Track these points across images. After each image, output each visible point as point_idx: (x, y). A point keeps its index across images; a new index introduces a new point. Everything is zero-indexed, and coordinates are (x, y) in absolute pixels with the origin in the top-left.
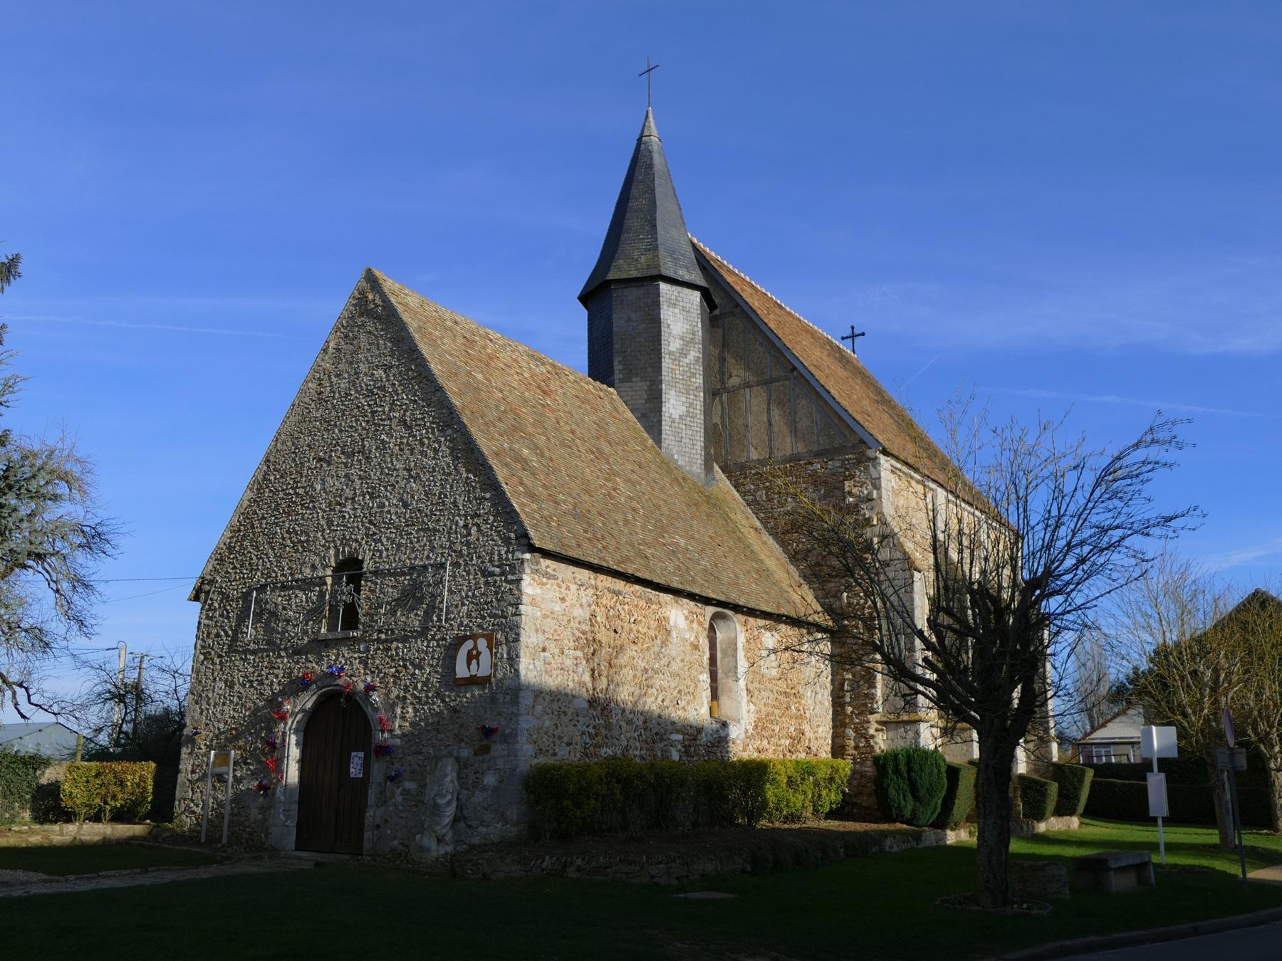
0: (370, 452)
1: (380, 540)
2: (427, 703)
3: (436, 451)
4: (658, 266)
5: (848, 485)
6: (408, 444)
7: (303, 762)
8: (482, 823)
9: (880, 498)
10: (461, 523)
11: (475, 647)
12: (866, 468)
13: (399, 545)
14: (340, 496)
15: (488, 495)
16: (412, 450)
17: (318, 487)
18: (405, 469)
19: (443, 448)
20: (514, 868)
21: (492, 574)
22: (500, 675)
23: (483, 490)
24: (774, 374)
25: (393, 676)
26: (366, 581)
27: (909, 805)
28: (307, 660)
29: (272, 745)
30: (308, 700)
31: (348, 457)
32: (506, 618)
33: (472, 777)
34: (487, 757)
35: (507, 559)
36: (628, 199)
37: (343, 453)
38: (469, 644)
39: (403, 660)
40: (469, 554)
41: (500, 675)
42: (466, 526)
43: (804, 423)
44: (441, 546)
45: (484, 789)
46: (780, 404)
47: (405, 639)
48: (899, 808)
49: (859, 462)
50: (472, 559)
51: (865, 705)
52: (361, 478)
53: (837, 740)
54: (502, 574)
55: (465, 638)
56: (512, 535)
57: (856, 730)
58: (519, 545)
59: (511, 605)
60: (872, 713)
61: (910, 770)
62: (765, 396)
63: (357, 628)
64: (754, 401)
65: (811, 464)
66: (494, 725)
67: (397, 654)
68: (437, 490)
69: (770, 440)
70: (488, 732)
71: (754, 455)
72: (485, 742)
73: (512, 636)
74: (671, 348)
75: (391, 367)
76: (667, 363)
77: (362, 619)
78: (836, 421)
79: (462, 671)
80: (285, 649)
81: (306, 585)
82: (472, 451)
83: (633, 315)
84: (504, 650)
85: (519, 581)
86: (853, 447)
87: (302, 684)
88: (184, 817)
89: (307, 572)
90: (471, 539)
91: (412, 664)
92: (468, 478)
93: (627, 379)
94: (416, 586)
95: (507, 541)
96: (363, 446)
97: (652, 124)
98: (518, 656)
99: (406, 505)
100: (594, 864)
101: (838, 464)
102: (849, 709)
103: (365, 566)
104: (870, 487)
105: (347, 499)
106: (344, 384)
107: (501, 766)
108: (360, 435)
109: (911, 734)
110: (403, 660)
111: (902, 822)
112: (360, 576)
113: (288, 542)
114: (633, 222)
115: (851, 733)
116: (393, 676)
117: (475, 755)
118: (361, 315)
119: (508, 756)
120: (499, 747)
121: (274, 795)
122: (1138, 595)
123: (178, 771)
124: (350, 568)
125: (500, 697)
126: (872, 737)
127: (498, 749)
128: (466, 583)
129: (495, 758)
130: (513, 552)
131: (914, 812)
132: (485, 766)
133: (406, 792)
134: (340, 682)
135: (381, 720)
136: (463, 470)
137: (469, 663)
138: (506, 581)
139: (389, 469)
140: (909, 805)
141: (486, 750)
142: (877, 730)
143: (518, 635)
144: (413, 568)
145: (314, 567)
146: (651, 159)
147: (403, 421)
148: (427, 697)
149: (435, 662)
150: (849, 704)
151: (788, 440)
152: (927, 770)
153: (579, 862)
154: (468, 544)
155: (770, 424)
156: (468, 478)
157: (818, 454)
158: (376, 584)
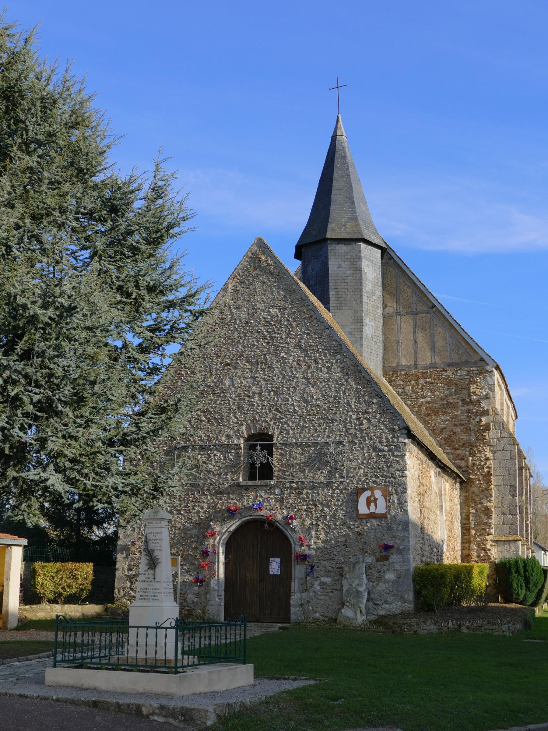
0: (272, 363)
1: (286, 423)
2: (334, 529)
3: (329, 369)
4: (360, 232)
5: (473, 387)
6: (304, 361)
7: (226, 564)
8: (386, 602)
9: (494, 397)
10: (354, 417)
11: (373, 495)
12: (485, 377)
13: (303, 427)
14: (248, 391)
15: (375, 401)
16: (309, 367)
17: (228, 383)
18: (304, 378)
19: (335, 367)
20: (432, 628)
21: (382, 451)
22: (393, 513)
23: (370, 397)
24: (419, 309)
25: (305, 511)
26: (277, 449)
27: (523, 593)
28: (229, 498)
29: (205, 553)
30: (233, 525)
31: (252, 365)
32: (395, 478)
33: (376, 575)
34: (386, 563)
35: (393, 442)
36: (331, 180)
37: (247, 362)
38: (368, 493)
39: (313, 500)
40: (362, 437)
41: (393, 513)
42: (358, 419)
43: (440, 344)
44: (339, 430)
45: (386, 582)
46: (423, 329)
47: (313, 488)
48: (518, 594)
49: (480, 373)
50: (365, 440)
51: (485, 529)
52: (265, 380)
53: (464, 551)
54: (389, 451)
55: (364, 490)
56: (396, 427)
57: (478, 545)
58: (401, 433)
59: (399, 470)
60: (489, 534)
61: (526, 571)
62: (411, 323)
63: (272, 479)
64: (403, 326)
65: (446, 371)
66: (391, 543)
67: (308, 497)
68: (333, 393)
69: (416, 353)
70: (387, 548)
71: (403, 362)
72: (384, 553)
73: (400, 490)
74: (367, 289)
75: (285, 308)
76: (365, 299)
77: (276, 474)
78: (463, 344)
79: (363, 509)
80: (208, 490)
81: (225, 449)
82: (360, 371)
83: (343, 264)
84: (395, 498)
85: (403, 456)
86: (475, 362)
87: (231, 513)
88: (124, 600)
89: (223, 439)
90: (363, 427)
91: (321, 504)
92: (357, 388)
93: (339, 307)
94: (320, 455)
95: (393, 431)
96: (266, 360)
97: (341, 123)
98: (406, 502)
99: (306, 401)
100: (475, 625)
101: (465, 373)
102: (473, 532)
103: (275, 438)
104: (487, 390)
105: (254, 393)
106: (244, 315)
107: (398, 568)
108: (262, 351)
109: (513, 548)
110: (313, 500)
111: (517, 603)
112: (271, 446)
113: (204, 418)
114: (336, 196)
115: (474, 547)
116: (305, 511)
117: (377, 561)
118: (255, 269)
119: (403, 562)
120: (395, 556)
121: (208, 585)
122: (69, 388)
123: (115, 570)
124: (261, 440)
125: (395, 526)
126: (489, 550)
127: (394, 557)
128: (361, 455)
129: (393, 563)
130: (398, 438)
131: (525, 597)
132: (386, 568)
133: (322, 584)
134: (262, 513)
135: (300, 538)
136: (353, 383)
137: (368, 505)
138: (393, 455)
139: (290, 377)
140: (523, 593)
141: (387, 558)
142: (491, 546)
143: (406, 489)
144: (316, 444)
145: (228, 437)
146: (345, 152)
147: (298, 345)
148: (336, 525)
149: (340, 503)
150: (473, 529)
151: (429, 354)
152: (535, 571)
153: (467, 623)
154: (361, 431)
155: (416, 342)
156: (357, 388)
157: (450, 365)
158: (286, 451)
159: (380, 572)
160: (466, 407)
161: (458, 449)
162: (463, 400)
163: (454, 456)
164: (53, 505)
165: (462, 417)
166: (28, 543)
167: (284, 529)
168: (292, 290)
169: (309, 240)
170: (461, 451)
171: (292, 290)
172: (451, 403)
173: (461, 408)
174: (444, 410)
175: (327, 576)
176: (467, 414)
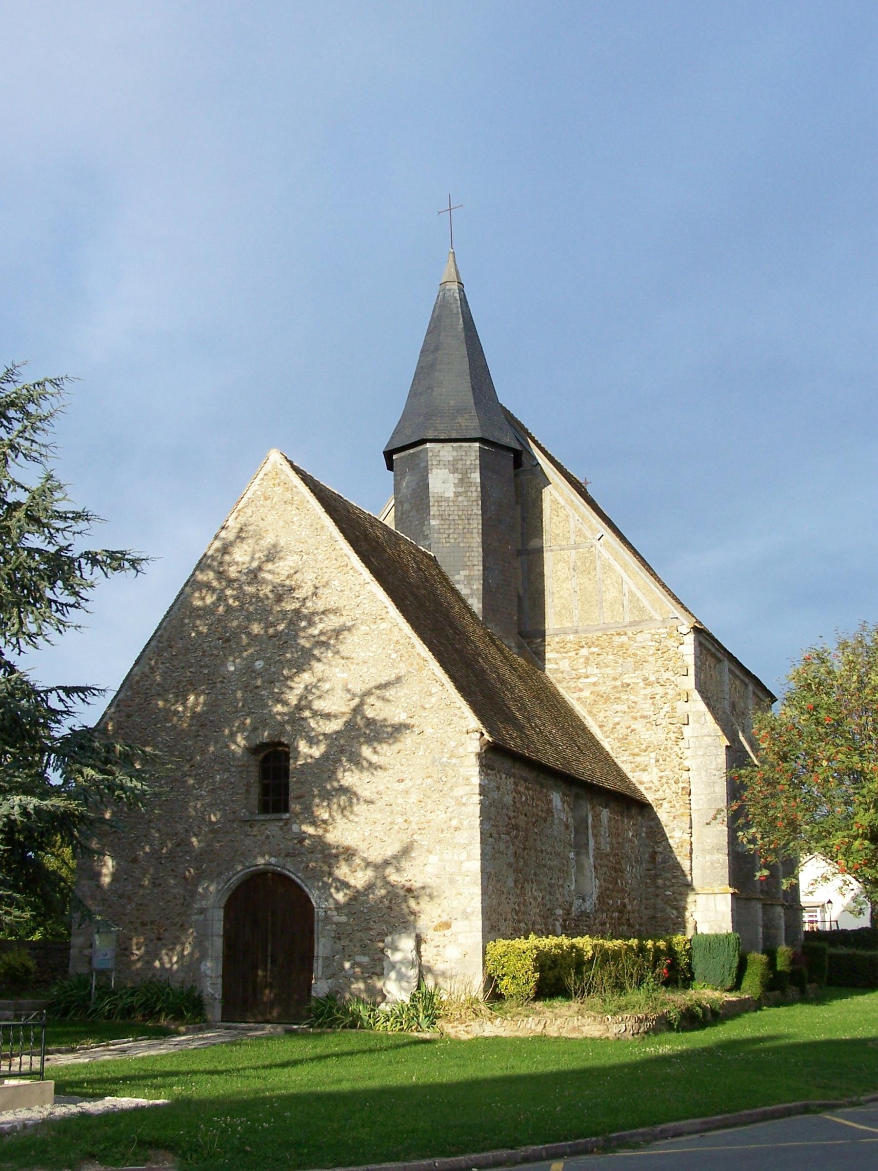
34: (448, 932)
159: (438, 946)
160: (649, 690)
161: (637, 755)
162: (645, 679)
163: (633, 765)
164: (773, 879)
165: (645, 706)
166: (781, 972)
167: (303, 885)
168: (319, 527)
169: (398, 444)
170: (643, 759)
171: (319, 527)
172: (628, 685)
173: (643, 692)
174: (618, 695)
175: (364, 954)
176: (651, 701)
